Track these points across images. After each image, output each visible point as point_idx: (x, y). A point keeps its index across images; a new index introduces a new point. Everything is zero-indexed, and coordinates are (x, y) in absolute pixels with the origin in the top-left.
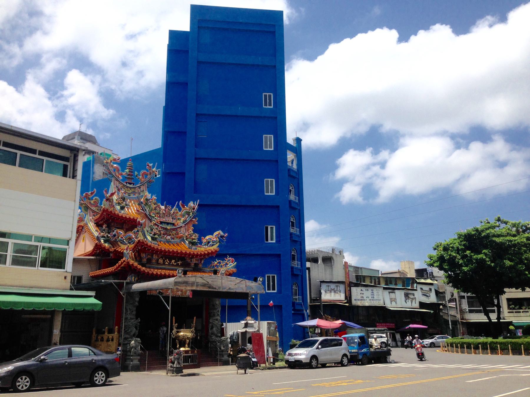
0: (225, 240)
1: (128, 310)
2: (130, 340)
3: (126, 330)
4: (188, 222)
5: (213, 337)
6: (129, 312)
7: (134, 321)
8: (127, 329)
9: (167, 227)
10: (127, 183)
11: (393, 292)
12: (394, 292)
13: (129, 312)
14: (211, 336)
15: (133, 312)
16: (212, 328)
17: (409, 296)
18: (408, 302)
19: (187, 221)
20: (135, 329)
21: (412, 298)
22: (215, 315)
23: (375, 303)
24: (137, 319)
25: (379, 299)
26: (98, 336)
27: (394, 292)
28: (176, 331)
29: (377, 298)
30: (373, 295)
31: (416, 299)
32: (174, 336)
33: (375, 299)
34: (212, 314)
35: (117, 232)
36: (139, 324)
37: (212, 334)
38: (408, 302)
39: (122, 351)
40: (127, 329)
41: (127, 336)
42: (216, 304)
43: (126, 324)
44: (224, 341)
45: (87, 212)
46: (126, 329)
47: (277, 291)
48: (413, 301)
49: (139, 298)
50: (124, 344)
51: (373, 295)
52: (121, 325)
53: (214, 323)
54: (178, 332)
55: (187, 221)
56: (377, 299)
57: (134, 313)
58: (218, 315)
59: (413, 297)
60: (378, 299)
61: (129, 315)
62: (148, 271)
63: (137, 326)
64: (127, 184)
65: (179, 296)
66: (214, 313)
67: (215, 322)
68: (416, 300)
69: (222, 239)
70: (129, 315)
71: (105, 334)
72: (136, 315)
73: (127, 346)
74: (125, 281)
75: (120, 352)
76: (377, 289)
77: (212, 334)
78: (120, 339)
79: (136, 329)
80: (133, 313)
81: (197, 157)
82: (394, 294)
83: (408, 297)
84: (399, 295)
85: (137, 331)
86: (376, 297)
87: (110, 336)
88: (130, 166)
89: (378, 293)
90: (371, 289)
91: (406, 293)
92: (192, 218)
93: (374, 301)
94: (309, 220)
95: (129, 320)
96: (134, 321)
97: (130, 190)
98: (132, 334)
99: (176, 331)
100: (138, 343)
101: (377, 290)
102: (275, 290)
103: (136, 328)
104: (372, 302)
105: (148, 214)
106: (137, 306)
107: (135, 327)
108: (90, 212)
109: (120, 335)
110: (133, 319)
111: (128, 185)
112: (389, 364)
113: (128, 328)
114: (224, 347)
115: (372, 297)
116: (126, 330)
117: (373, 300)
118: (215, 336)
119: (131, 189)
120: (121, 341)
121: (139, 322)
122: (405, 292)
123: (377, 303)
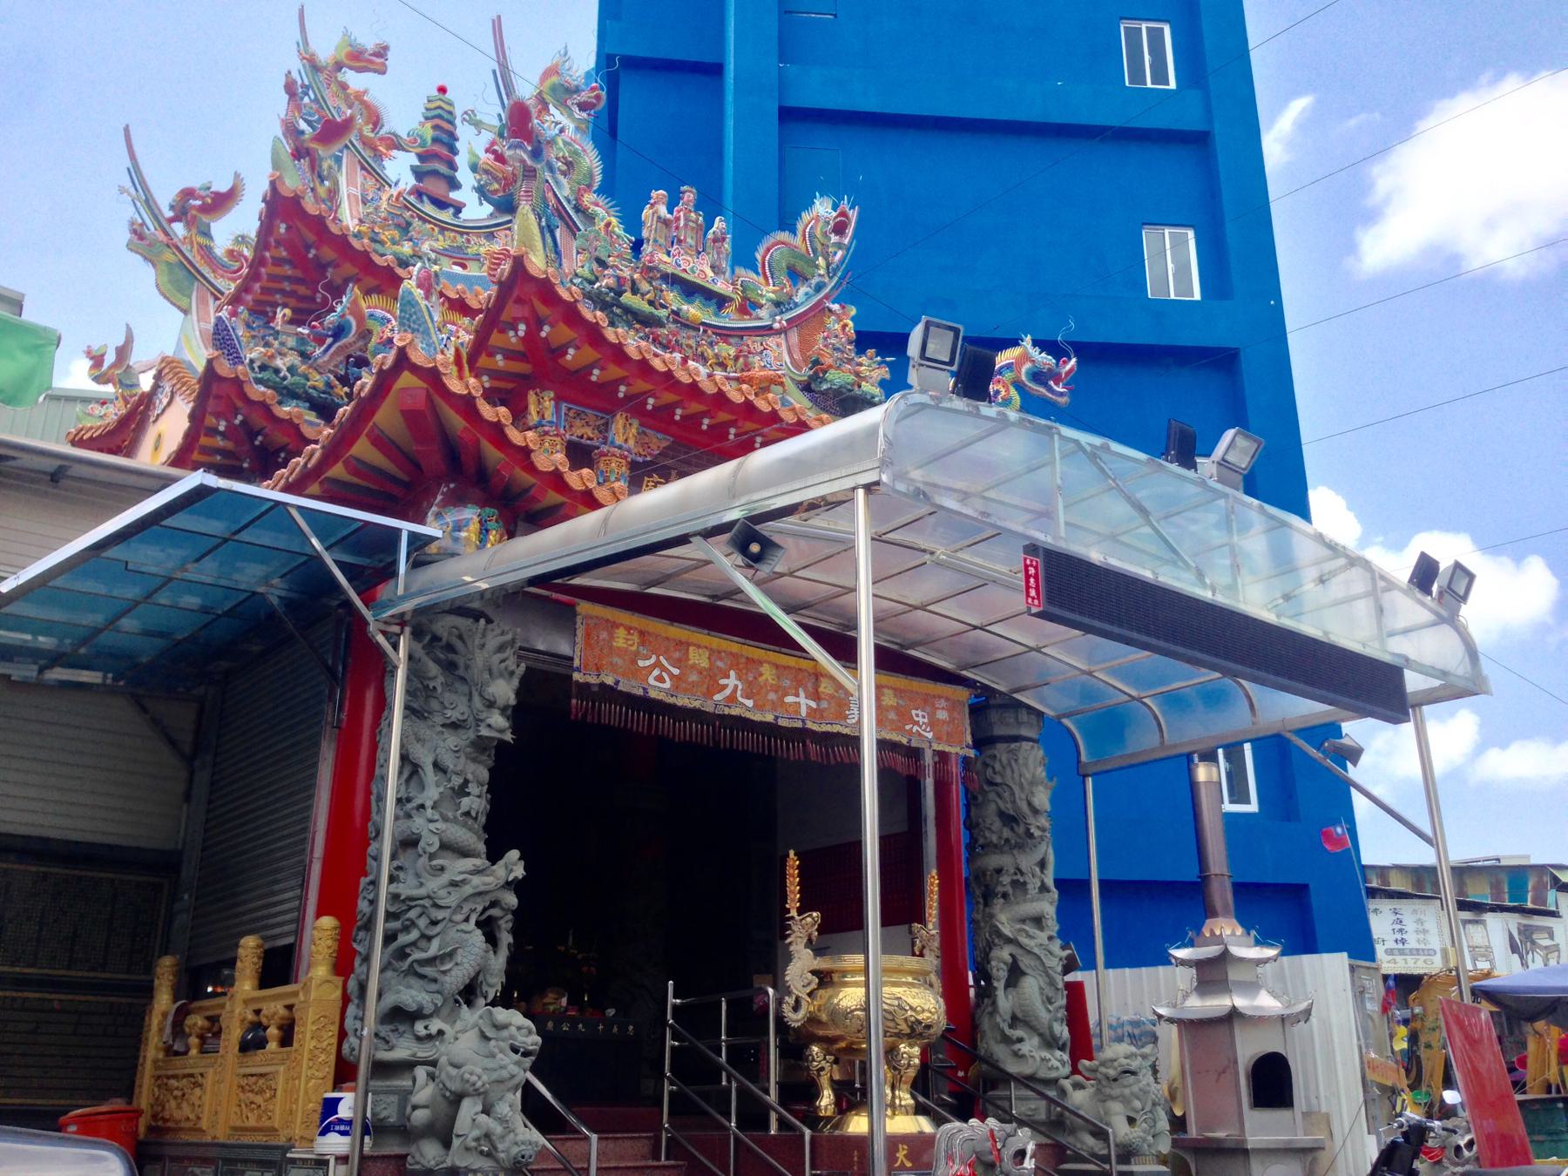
0: (1061, 394)
1: (429, 774)
2: (441, 1033)
3: (403, 939)
4: (805, 313)
5: (1025, 1048)
6: (432, 793)
7: (478, 872)
8: (414, 935)
9: (685, 307)
10: (425, 198)
11: (1476, 922)
12: (1483, 922)
13: (432, 793)
14: (1007, 1040)
15: (462, 791)
16: (1015, 974)
17: (1534, 936)
18: (1533, 961)
19: (796, 305)
20: (478, 937)
21: (1546, 947)
22: (1025, 883)
23: (1413, 965)
24: (494, 855)
25: (1428, 947)
26: (188, 1013)
27: (1483, 922)
28: (814, 972)
29: (1418, 946)
30: (1401, 931)
31: (1559, 951)
32: (796, 1008)
33: (1411, 950)
34: (1006, 879)
35: (355, 309)
36: (511, 900)
37: (1015, 1021)
38: (1533, 961)
39: (366, 1131)
40: (414, 935)
41: (412, 995)
42: (1030, 804)
43: (405, 890)
44: (1133, 1073)
45: (186, 300)
46: (406, 929)
47: (1260, 808)
48: (1551, 961)
49: (516, 682)
50: (382, 1069)
51: (1401, 931)
52: (363, 905)
53: (1023, 940)
54: (825, 979)
55: (796, 305)
56: (1418, 950)
57: (476, 801)
58: (1044, 888)
59: (1547, 943)
60: (1423, 950)
61: (429, 812)
62: (591, 485)
63: (495, 912)
64: (422, 201)
65: (799, 725)
66: (1019, 871)
67: (1031, 937)
68: (1559, 957)
69: (1042, 390)
70: (429, 812)
71: (268, 1046)
72: (486, 828)
73: (407, 1083)
74: (406, 527)
75: (346, 1140)
76: (1417, 907)
77: (1015, 1021)
78: (349, 1023)
79: (492, 940)
80: (466, 802)
81: (793, 102)
82: (1480, 928)
83: (1533, 943)
84: (1497, 929)
85: (499, 962)
86: (1412, 943)
87: (274, 1005)
88: (439, 117)
89: (1420, 922)
90: (1390, 907)
91: (1525, 926)
92: (826, 297)
93: (1408, 958)
94: (1315, 488)
95: (432, 857)
96: (478, 872)
97: (441, 237)
98: (456, 977)
99: (814, 972)
100: (515, 1050)
101: (1415, 911)
102: (1248, 802)
103: (488, 927)
104: (1399, 958)
105: (569, 201)
106: (501, 744)
107: (478, 924)
108: (202, 302)
109: (352, 984)
110: (465, 853)
111: (429, 208)
112: (24, 1143)
113: (423, 922)
114: (1131, 1121)
115: (1396, 941)
116: (403, 939)
117: (1402, 952)
118: (1036, 1040)
119: (442, 230)
120: (364, 1049)
121: (516, 886)
122: (1519, 924)
123: (1420, 964)
